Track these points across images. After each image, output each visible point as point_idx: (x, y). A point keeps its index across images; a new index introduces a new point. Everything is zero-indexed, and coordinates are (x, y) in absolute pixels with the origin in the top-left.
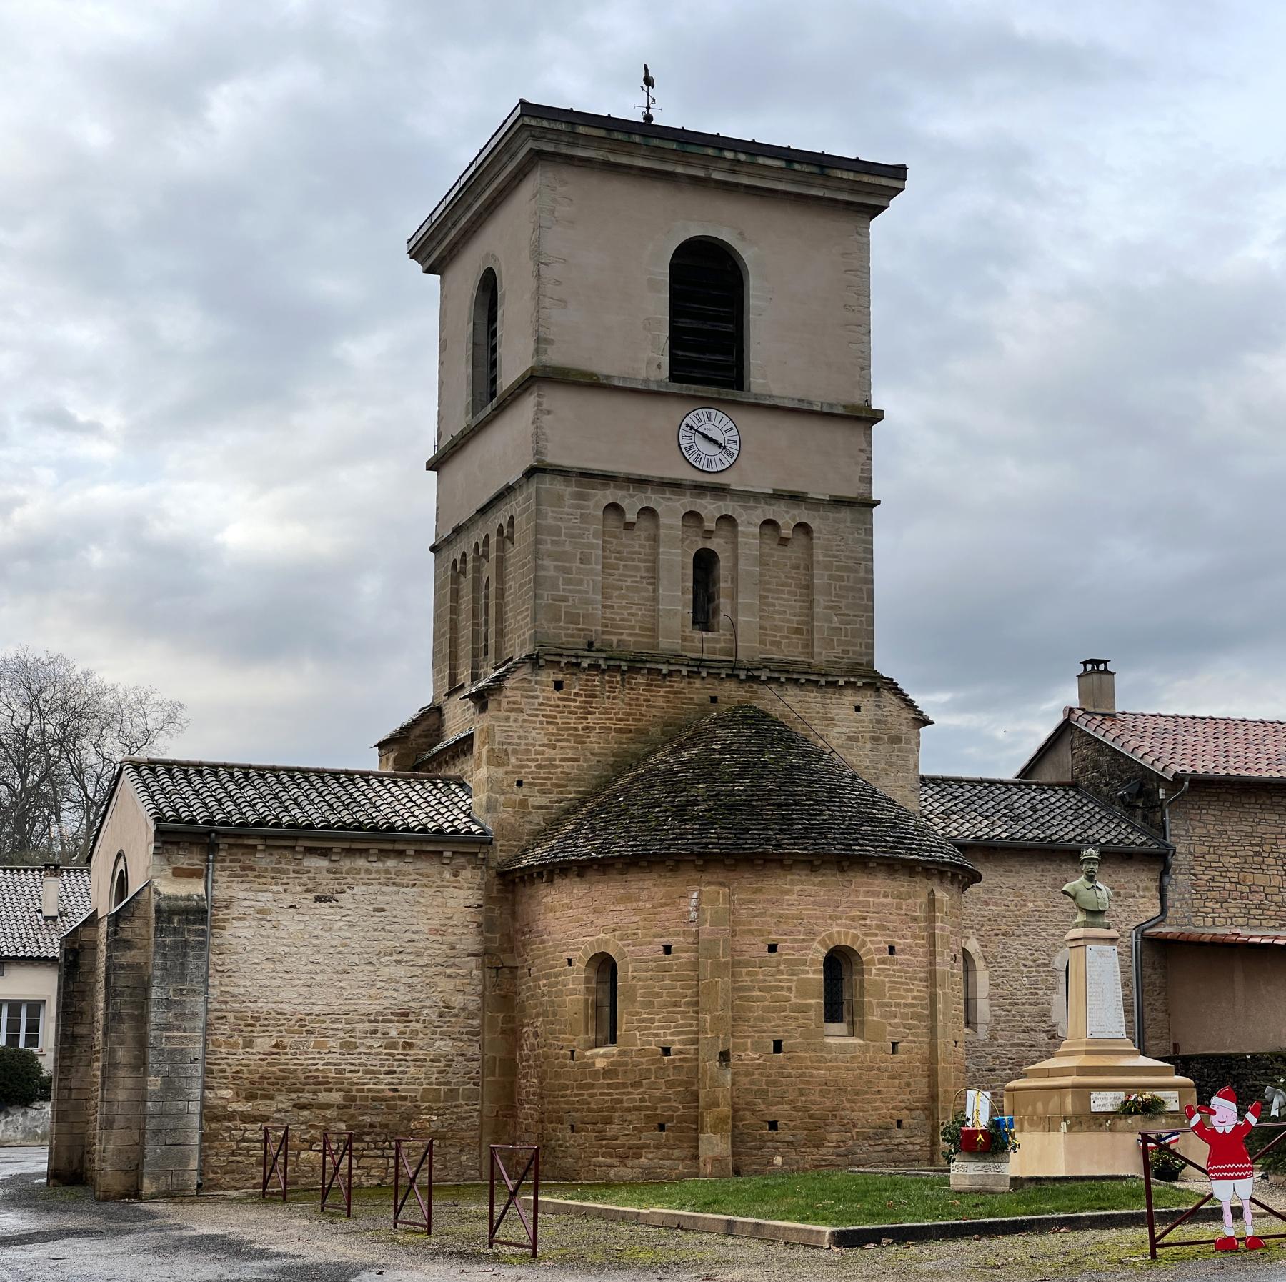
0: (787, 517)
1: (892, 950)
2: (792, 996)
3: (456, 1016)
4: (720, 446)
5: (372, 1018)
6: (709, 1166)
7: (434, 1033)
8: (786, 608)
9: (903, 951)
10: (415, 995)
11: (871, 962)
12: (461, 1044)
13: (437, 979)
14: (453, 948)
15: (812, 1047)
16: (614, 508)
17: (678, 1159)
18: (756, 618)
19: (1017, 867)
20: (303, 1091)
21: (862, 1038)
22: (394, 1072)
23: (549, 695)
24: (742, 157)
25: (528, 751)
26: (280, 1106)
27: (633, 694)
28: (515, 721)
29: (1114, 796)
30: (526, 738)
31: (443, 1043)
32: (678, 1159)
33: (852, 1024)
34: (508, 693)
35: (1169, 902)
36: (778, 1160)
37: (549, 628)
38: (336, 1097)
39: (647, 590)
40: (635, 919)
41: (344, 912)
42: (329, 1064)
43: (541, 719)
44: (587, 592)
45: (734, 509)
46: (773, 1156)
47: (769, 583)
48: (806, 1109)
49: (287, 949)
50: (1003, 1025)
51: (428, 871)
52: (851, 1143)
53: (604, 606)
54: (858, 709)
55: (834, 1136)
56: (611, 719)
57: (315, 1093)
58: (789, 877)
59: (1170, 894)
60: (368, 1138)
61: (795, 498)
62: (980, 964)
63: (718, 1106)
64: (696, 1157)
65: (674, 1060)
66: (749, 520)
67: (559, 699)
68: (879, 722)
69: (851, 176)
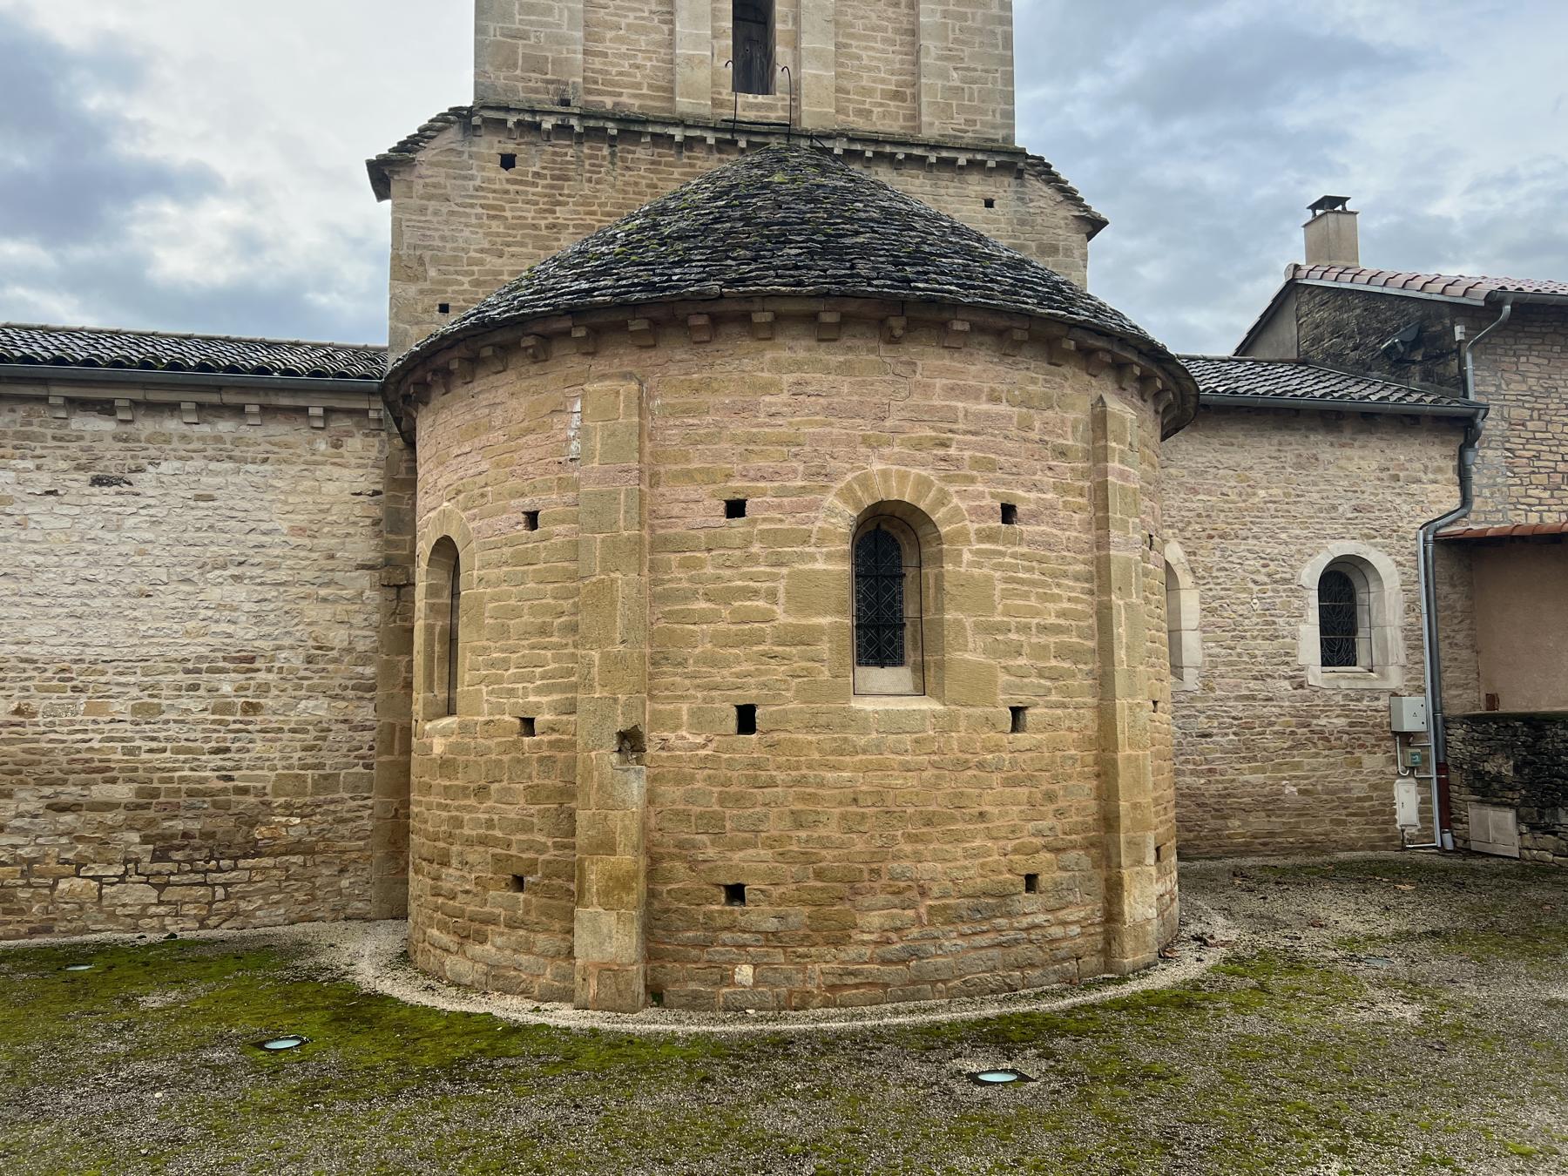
1: (1008, 513)
3: (335, 661)
5: (190, 666)
6: (593, 983)
7: (299, 687)
8: (878, 63)
9: (1034, 516)
10: (265, 630)
11: (962, 536)
12: (343, 704)
13: (304, 603)
14: (332, 557)
15: (823, 720)
17: (543, 954)
19: (1241, 438)
20: (65, 782)
21: (940, 698)
22: (227, 750)
23: (492, 175)
25: (456, 259)
26: (23, 807)
27: (629, 176)
28: (436, 213)
29: (1383, 353)
31: (312, 703)
32: (543, 954)
33: (921, 669)
34: (423, 170)
35: (1475, 490)
36: (745, 973)
37: (500, 79)
38: (123, 792)
39: (656, 30)
40: (484, 466)
41: (143, 501)
42: (112, 739)
43: (480, 210)
46: (734, 963)
48: (807, 858)
49: (40, 559)
50: (1223, 669)
51: (290, 439)
52: (915, 932)
53: (586, 52)
54: (989, 204)
55: (875, 919)
56: (593, 213)
57: (86, 785)
58: (769, 355)
59: (1475, 478)
60: (178, 856)
62: (1185, 580)
63: (612, 850)
64: (570, 954)
65: (539, 745)
67: (508, 181)
68: (1022, 222)
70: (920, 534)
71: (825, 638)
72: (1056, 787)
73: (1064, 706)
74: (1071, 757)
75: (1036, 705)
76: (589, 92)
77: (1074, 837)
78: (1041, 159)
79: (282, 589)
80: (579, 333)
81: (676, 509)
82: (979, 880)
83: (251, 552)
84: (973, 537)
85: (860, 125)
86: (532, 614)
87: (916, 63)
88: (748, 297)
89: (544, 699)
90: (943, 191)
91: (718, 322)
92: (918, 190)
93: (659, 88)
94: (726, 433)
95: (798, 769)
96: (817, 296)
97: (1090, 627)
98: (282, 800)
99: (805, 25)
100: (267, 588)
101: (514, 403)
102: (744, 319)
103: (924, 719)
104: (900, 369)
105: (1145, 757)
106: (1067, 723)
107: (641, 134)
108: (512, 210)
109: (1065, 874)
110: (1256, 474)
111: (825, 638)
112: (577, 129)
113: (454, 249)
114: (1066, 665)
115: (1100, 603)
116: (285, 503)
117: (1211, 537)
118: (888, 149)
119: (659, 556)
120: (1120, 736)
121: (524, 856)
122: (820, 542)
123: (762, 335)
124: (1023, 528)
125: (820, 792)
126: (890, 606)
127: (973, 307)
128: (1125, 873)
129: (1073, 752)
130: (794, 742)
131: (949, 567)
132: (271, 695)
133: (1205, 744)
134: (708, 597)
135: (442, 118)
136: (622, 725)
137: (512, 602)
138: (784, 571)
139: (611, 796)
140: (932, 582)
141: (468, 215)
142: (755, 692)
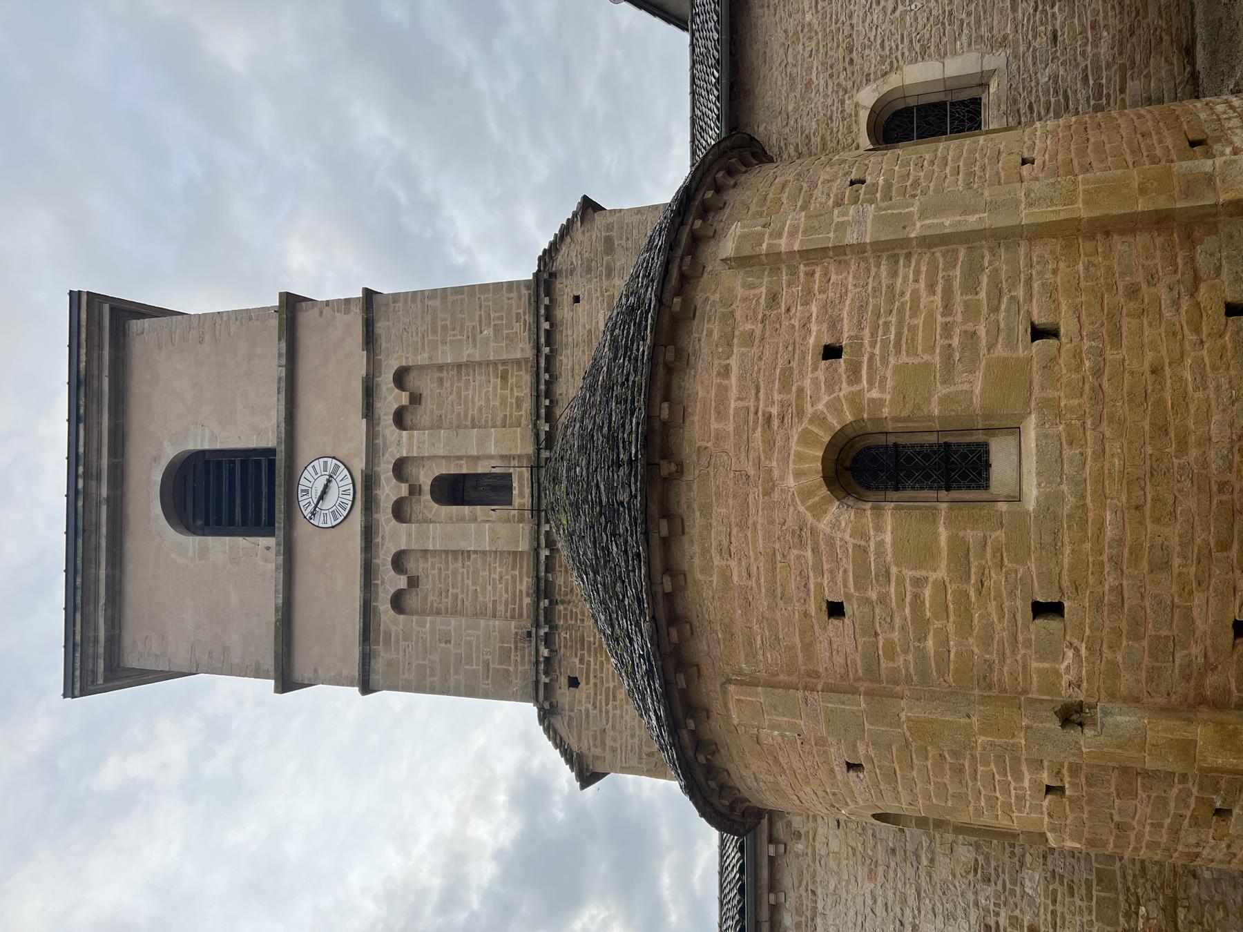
0: (390, 398)
1: (832, 352)
2: (933, 576)
3: (987, 859)
4: (329, 481)
7: (1013, 893)
9: (834, 324)
10: (960, 913)
11: (855, 399)
12: (1028, 858)
14: (893, 851)
15: (1047, 538)
16: (398, 602)
18: (496, 440)
24: (81, 469)
28: (614, 740)
30: (633, 728)
31: (1027, 883)
33: (991, 430)
34: (585, 747)
43: (610, 706)
44: (478, 638)
45: (388, 462)
47: (459, 414)
48: (1205, 557)
51: (795, 872)
53: (494, 616)
54: (577, 299)
58: (698, 576)
61: (370, 392)
66: (397, 444)
67: (587, 683)
68: (589, 270)
69: (83, 351)
70: (854, 435)
71: (961, 534)
72: (1121, 286)
73: (1029, 280)
74: (1087, 269)
75: (1029, 313)
76: (521, 615)
77: (1180, 261)
78: (540, 259)
79: (923, 894)
80: (691, 724)
81: (839, 660)
82: (1232, 372)
83: (891, 914)
84: (855, 388)
85: (527, 405)
86: (943, 776)
87: (480, 363)
88: (652, 596)
89: (1027, 776)
90: (570, 339)
91: (675, 618)
92: (570, 387)
93: (514, 562)
94: (767, 614)
95: (1102, 564)
96: (647, 541)
97: (944, 255)
98: (1122, 920)
99: (461, 453)
100: (922, 907)
101: (754, 767)
102: (670, 598)
103: (1046, 436)
104: (704, 461)
105: (1086, 181)
106: (1049, 275)
107: (546, 581)
108: (608, 682)
109: (1225, 270)
110: (791, 25)
111: (961, 534)
112: (546, 630)
113: (640, 728)
114: (985, 280)
115: (919, 246)
116: (848, 881)
117: (852, 60)
118: (542, 387)
119: (884, 676)
120: (1062, 216)
121: (1193, 806)
122: (864, 536)
123: (682, 583)
124: (845, 335)
125: (1128, 543)
126: (927, 457)
127: (649, 404)
128: (1223, 198)
129: (1081, 267)
130: (1072, 567)
131: (886, 412)
132: (1020, 916)
133: (1063, 37)
134: (922, 638)
135: (547, 730)
136: (1055, 724)
137: (932, 788)
138: (894, 570)
139: (1130, 739)
140: (900, 425)
141: (614, 716)
142: (1018, 602)
